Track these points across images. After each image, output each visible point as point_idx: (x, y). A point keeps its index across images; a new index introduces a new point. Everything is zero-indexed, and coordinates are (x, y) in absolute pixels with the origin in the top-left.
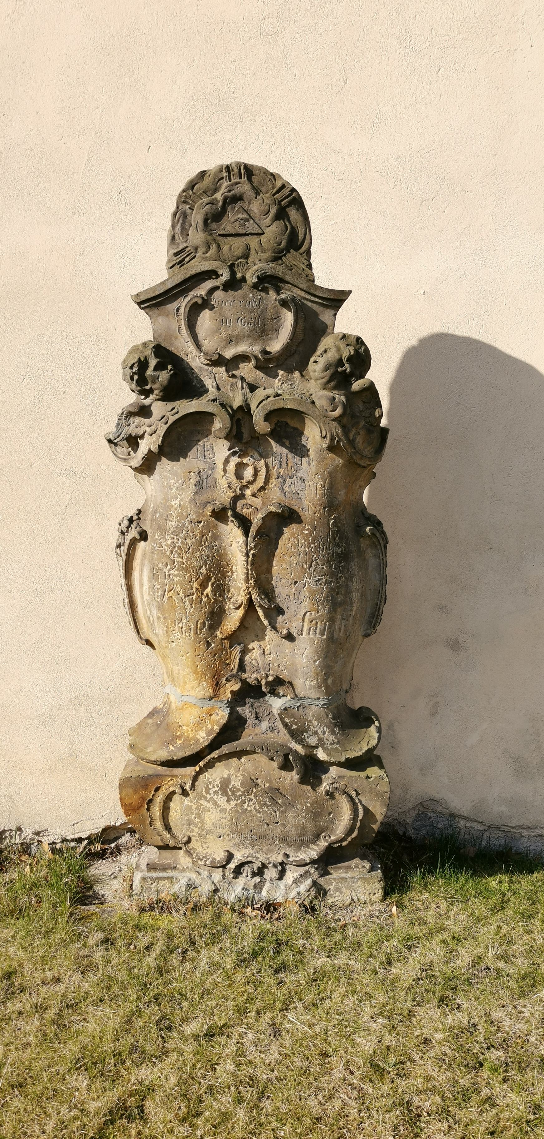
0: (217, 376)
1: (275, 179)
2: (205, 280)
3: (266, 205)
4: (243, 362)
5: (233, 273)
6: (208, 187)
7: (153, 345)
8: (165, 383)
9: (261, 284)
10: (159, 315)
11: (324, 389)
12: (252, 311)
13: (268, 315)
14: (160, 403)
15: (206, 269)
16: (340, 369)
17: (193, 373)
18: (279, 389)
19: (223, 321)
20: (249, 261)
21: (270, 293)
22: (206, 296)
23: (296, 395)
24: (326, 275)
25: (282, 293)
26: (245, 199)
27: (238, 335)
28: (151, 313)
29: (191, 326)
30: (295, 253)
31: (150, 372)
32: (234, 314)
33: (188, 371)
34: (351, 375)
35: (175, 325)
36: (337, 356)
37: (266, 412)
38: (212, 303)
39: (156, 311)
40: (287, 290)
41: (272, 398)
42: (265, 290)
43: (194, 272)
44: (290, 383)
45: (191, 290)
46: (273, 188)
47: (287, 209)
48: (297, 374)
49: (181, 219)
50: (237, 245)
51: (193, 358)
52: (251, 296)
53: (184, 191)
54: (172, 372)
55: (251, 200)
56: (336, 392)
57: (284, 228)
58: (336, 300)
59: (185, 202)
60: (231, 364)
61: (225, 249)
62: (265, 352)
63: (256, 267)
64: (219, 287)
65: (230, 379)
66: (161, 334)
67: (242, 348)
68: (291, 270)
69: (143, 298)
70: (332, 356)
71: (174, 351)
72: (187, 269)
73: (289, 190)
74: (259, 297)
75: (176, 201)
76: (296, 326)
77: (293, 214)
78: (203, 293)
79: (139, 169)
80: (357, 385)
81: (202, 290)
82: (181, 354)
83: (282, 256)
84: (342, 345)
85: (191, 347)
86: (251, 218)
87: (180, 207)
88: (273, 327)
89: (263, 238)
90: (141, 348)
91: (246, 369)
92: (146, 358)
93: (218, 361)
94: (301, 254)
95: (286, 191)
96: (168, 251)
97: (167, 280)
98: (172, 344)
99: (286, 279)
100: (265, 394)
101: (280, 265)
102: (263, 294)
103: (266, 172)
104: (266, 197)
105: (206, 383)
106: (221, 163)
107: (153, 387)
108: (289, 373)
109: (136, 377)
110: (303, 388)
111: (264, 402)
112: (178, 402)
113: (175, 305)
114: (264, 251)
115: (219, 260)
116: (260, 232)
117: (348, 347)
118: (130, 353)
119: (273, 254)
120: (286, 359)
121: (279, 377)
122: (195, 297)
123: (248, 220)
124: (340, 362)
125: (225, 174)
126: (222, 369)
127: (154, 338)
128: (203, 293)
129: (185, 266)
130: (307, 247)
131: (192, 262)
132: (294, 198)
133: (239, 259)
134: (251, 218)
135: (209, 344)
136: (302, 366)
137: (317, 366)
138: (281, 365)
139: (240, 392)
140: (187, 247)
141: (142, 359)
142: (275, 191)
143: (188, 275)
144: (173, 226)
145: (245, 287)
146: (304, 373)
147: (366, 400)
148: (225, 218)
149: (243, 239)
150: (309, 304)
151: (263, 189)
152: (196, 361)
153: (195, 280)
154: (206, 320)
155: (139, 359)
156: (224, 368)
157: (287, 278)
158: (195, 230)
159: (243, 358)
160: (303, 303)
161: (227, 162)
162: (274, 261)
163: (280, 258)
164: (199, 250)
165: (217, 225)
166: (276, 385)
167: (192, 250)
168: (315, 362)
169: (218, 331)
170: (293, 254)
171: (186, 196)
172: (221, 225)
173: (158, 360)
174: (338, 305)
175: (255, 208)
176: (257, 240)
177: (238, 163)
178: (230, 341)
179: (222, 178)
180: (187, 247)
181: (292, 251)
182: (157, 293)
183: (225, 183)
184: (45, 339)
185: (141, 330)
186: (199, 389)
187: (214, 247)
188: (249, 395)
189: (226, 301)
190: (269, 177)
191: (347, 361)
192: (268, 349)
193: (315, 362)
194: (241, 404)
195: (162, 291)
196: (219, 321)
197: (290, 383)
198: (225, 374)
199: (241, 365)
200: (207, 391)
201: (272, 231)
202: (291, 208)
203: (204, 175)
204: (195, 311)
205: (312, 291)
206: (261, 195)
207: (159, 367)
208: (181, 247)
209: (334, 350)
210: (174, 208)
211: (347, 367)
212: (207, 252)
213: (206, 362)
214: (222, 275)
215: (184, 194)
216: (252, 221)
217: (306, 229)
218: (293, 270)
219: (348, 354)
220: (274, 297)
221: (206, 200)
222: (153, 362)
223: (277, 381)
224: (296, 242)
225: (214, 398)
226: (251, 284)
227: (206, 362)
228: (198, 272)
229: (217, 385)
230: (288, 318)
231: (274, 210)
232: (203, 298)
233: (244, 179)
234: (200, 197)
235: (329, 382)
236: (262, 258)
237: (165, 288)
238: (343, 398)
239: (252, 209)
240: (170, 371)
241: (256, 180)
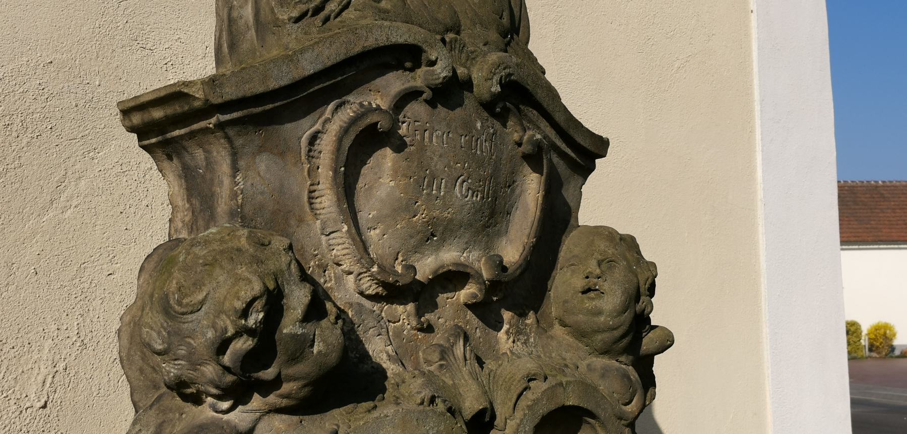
2: (384, 68)
10: (261, 149)
14: (279, 422)
19: (421, 179)
21: (510, 123)
27: (451, 220)
28: (239, 142)
29: (347, 188)
32: (450, 167)
37: (537, 421)
48: (531, 319)
52: (479, 125)
60: (421, 294)
64: (422, 93)
66: (261, 207)
67: (449, 255)
93: (392, 292)
112: (336, 412)
113: (305, 128)
121: (506, 327)
143: (357, 49)
154: (383, 173)
155: (267, 289)
169: (407, 208)
178: (432, 235)
195: (285, 82)
196: (416, 181)
223: (502, 335)
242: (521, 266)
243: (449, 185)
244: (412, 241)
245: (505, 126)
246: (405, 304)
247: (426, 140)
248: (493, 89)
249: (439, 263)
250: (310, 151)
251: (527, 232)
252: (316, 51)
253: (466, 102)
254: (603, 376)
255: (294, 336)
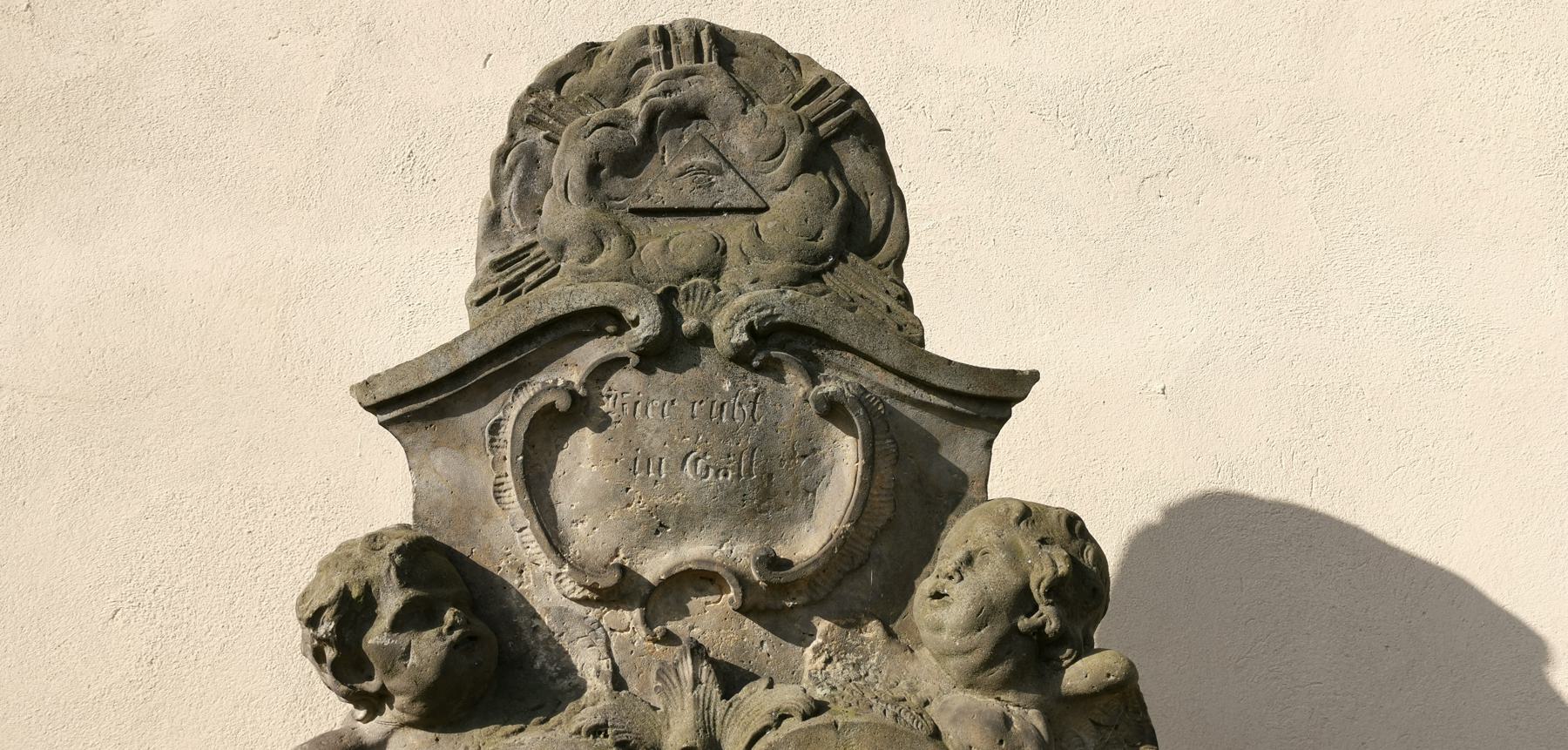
0: (614, 638)
1: (798, 67)
2: (582, 338)
3: (772, 132)
4: (701, 592)
5: (671, 317)
6: (603, 83)
7: (398, 543)
8: (429, 674)
9: (759, 350)
10: (436, 445)
11: (970, 686)
12: (731, 433)
13: (781, 447)
15: (584, 303)
16: (1023, 623)
17: (536, 629)
18: (818, 684)
19: (636, 463)
20: (721, 285)
21: (789, 377)
22: (585, 385)
23: (877, 710)
24: (958, 331)
25: (826, 378)
26: (711, 116)
27: (685, 507)
28: (410, 439)
30: (861, 263)
31: (377, 636)
32: (672, 442)
33: (522, 620)
34: (1062, 639)
35: (484, 477)
36: (1014, 581)
38: (604, 408)
39: (425, 435)
40: (839, 368)
41: (793, 724)
42: (773, 369)
43: (546, 314)
44: (852, 658)
45: (538, 370)
46: (794, 89)
47: (836, 146)
48: (873, 631)
49: (519, 167)
50: (688, 239)
51: (540, 581)
52: (727, 386)
53: (531, 91)
54: (457, 633)
55: (728, 119)
56: (1009, 696)
57: (826, 193)
58: (991, 398)
59: (530, 121)
60: (661, 600)
61: (650, 249)
62: (772, 563)
63: (743, 300)
64: (626, 360)
65: (659, 648)
66: (439, 505)
67: (695, 550)
68: (853, 310)
69: (384, 392)
70: (992, 576)
71: (479, 558)
72: (525, 306)
73: (839, 92)
74: (754, 390)
75: (507, 120)
76: (872, 479)
77: (851, 156)
78: (575, 377)
79: (460, 104)
80: (1079, 675)
81: (572, 369)
82: (502, 568)
83: (824, 271)
84: (1026, 543)
85: (532, 546)
86: (730, 166)
87: (520, 135)
88: (795, 483)
89: (764, 222)
90: (358, 552)
91: (711, 619)
92: (367, 588)
93: (621, 590)
94: (880, 267)
95: (832, 97)
96: (478, 258)
97: (463, 337)
98: (473, 536)
99: (839, 338)
100: (773, 705)
101: (817, 295)
102: (766, 381)
103: (773, 49)
104: (774, 112)
105: (577, 661)
106: (640, 22)
107: (390, 685)
108: (848, 626)
109: (330, 653)
110: (894, 676)
111: (770, 737)
112: (476, 732)
113: (488, 413)
114: (767, 255)
115: (627, 280)
116: (755, 203)
117: (1045, 549)
118: (326, 565)
119: (797, 265)
120: (839, 583)
121: (818, 640)
122: (547, 388)
123: (720, 173)
124: (1023, 600)
125: (653, 49)
126: (632, 616)
127: (416, 517)
128: (575, 377)
129: (523, 296)
130: (895, 248)
131: (544, 285)
132: (855, 117)
133: (690, 277)
134: (730, 166)
135: (590, 536)
136: (890, 604)
137: (948, 604)
138: (822, 601)
139: (689, 696)
140: (533, 245)
141: (355, 593)
142: (797, 96)
143: (529, 324)
144: (496, 188)
145: (708, 359)
146: (895, 627)
147: (1103, 720)
148: (652, 165)
149: (706, 224)
150: (910, 412)
151: (765, 92)
152: (547, 590)
153: (550, 337)
154: (582, 461)
155: (345, 593)
156: (637, 613)
157: (842, 333)
158: (560, 199)
159: (700, 579)
160: (890, 411)
161: (664, 20)
162: (799, 284)
163: (817, 277)
164: (568, 253)
165: (627, 185)
166: (807, 667)
167: (549, 254)
168: (937, 595)
170: (855, 265)
171: (535, 105)
172: (640, 183)
173: (411, 592)
174: (998, 416)
175: (742, 140)
176: (747, 225)
177: (691, 21)
178: (659, 527)
179: (646, 61)
180: (533, 245)
181: (852, 257)
182: (429, 378)
183: (655, 73)
184: (186, 506)
185: (379, 488)
186: (553, 679)
187: (614, 245)
188: (720, 706)
189: (648, 401)
190: (782, 61)
191: (1047, 595)
192: (782, 552)
193: (937, 595)
194: (691, 743)
195: (443, 372)
196: (625, 464)
197: (852, 658)
198: (642, 632)
199: (695, 603)
200: (579, 689)
201: (793, 204)
202: (848, 142)
203: (595, 53)
204: (549, 429)
205: (921, 373)
206: (759, 105)
207: (411, 619)
208: (516, 245)
209: (999, 557)
210: (500, 136)
211: (1048, 617)
212: (592, 258)
213: (579, 593)
214: (636, 322)
215: (532, 100)
216: (730, 175)
217: (892, 200)
218: (859, 311)
219: (1048, 572)
220: (801, 391)
221: (597, 115)
222: (391, 602)
223: (809, 652)
224: (864, 234)
225: (600, 720)
226: (728, 350)
227: (579, 593)
228: (559, 312)
229: (615, 668)
230: (845, 455)
231: (796, 145)
232: (573, 394)
233: (710, 63)
234: (580, 106)
235: (988, 664)
236: (762, 273)
237: (455, 363)
238: (1035, 718)
239: (734, 141)
240: (451, 630)
241: (743, 69)
242: (816, 561)
243: (673, 465)
244: (635, 534)
245: (782, 381)
246: (631, 610)
247: (638, 413)
248: (734, 340)
249: (678, 560)
250: (492, 441)
251: (839, 516)
252: (480, 334)
253: (705, 359)
254: (954, 720)
255: (380, 648)
